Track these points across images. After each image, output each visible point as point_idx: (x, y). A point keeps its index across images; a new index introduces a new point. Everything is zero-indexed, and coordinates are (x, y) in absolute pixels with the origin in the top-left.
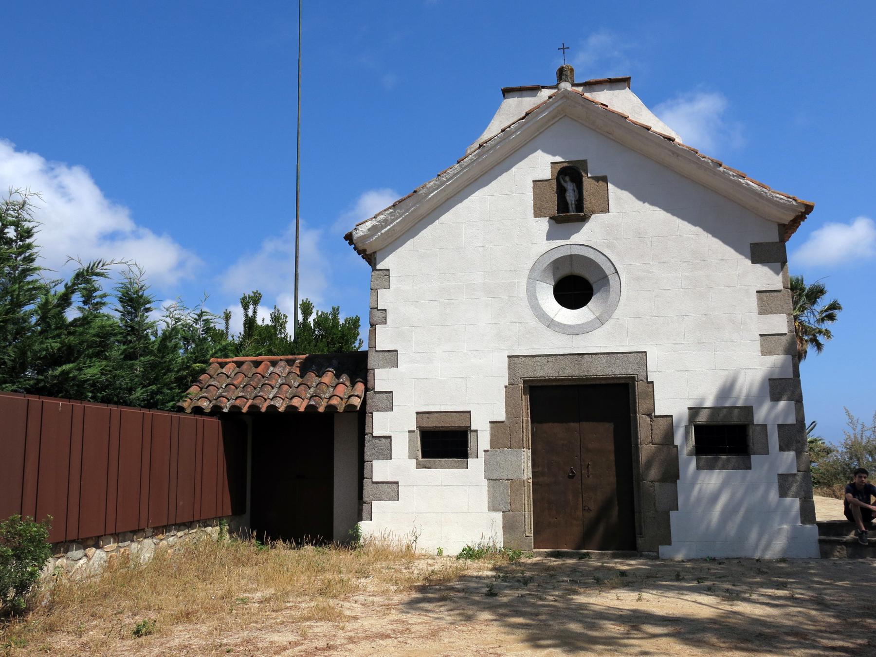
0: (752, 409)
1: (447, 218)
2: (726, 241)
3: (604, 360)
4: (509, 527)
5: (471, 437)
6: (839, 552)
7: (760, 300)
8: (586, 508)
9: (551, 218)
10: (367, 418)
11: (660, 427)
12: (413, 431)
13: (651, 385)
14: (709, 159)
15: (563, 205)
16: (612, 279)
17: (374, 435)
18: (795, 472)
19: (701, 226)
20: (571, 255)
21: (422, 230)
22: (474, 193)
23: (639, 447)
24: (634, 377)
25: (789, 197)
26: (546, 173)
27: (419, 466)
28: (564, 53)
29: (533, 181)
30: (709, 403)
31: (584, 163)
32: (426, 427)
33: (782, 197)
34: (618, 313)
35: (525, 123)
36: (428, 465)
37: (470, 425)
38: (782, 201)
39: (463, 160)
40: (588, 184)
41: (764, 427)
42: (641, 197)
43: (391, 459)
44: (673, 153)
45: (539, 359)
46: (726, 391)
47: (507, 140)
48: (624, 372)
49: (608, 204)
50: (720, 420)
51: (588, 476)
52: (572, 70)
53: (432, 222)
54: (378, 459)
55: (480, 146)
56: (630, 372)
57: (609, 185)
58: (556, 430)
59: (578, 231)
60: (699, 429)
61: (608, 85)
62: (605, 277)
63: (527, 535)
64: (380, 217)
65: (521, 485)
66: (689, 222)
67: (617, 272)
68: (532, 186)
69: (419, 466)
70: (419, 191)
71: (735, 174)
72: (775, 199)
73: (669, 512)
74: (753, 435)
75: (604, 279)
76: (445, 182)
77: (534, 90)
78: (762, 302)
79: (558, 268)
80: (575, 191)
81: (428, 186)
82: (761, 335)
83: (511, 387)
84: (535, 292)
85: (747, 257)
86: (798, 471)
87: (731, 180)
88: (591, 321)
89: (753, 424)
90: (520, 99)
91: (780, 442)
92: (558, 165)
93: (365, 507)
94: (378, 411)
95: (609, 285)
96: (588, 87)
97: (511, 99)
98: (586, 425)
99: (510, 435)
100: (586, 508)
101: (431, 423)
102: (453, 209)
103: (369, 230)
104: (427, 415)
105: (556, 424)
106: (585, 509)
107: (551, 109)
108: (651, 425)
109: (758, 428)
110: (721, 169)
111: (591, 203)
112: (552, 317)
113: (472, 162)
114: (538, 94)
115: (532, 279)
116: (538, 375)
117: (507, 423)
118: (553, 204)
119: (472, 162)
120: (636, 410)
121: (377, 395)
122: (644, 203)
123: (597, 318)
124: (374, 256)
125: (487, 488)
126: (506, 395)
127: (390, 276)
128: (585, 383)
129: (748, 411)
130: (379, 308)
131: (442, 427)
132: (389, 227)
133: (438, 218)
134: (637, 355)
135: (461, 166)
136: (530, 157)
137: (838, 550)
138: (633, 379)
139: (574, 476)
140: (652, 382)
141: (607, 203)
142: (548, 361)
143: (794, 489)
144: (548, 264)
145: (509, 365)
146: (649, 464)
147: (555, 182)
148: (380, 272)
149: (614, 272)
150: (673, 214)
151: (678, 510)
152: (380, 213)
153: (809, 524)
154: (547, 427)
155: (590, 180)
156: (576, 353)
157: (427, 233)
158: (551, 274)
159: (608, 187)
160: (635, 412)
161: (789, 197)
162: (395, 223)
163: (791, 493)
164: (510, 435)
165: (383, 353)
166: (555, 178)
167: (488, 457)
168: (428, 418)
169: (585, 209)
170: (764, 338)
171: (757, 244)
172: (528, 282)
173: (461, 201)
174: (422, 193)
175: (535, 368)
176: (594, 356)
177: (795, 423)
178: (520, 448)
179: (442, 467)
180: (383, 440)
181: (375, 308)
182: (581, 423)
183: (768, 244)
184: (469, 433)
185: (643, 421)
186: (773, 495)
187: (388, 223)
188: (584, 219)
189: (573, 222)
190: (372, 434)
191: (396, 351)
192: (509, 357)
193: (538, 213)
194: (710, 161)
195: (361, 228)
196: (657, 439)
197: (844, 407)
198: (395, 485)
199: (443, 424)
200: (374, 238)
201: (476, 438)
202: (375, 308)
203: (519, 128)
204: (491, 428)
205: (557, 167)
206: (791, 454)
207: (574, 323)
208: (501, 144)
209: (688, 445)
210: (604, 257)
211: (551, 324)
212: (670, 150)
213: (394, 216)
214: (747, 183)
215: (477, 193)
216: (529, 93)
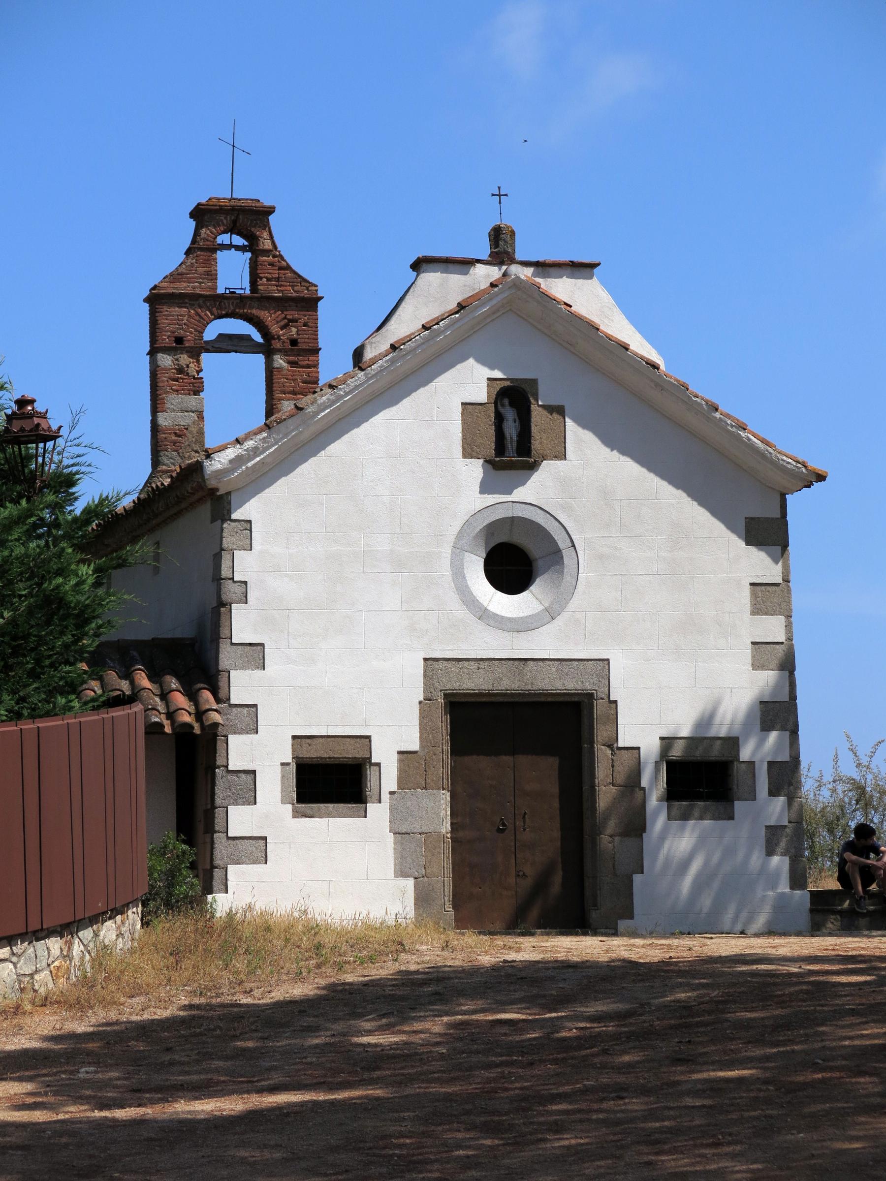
0: (738, 741)
1: (337, 448)
2: (714, 513)
3: (554, 669)
4: (422, 899)
5: (371, 774)
6: (833, 923)
7: (754, 595)
8: (521, 873)
9: (486, 461)
10: (219, 743)
11: (624, 762)
12: (288, 764)
13: (613, 706)
14: (702, 399)
15: (500, 446)
16: (567, 554)
17: (231, 768)
18: (786, 823)
19: (685, 490)
20: (513, 517)
21: (301, 464)
22: (377, 414)
23: (596, 789)
24: (592, 694)
25: (798, 462)
26: (480, 394)
27: (297, 814)
28: (500, 203)
29: (463, 404)
30: (685, 732)
31: (534, 382)
32: (307, 758)
33: (790, 460)
34: (575, 603)
35: (458, 320)
36: (309, 812)
37: (369, 756)
38: (789, 466)
39: (370, 366)
40: (538, 415)
41: (751, 764)
42: (610, 441)
43: (255, 803)
44: (657, 385)
45: (466, 664)
46: (706, 721)
47: (431, 342)
48: (579, 686)
49: (565, 448)
50: (698, 754)
51: (524, 830)
52: (513, 233)
53: (315, 454)
54: (236, 803)
55: (393, 347)
56: (588, 687)
57: (567, 420)
58: (483, 764)
59: (523, 483)
60: (673, 767)
61: (569, 270)
62: (558, 552)
63: (447, 909)
64: (248, 443)
65: (440, 841)
66: (671, 482)
67: (574, 546)
68: (460, 410)
69: (297, 814)
70: (307, 409)
71: (734, 424)
72: (781, 462)
73: (632, 876)
74: (738, 771)
75: (555, 556)
76: (342, 397)
77: (465, 264)
78: (756, 598)
79: (493, 534)
80: (515, 422)
81: (319, 402)
82: (753, 643)
83: (427, 703)
84: (463, 568)
85: (740, 537)
86: (790, 822)
87: (728, 431)
88: (538, 614)
89: (738, 760)
90: (444, 275)
91: (769, 784)
92: (498, 382)
93: (217, 873)
94: (235, 733)
95: (563, 564)
96: (540, 269)
97: (432, 274)
98: (523, 760)
99: (426, 771)
100: (521, 873)
101: (312, 753)
102: (346, 436)
103: (231, 461)
104: (308, 741)
105: (481, 757)
106: (519, 875)
107: (494, 302)
108: (613, 760)
109: (743, 766)
110: (717, 415)
111: (541, 443)
112: (485, 604)
113: (381, 370)
114: (471, 272)
115: (458, 548)
116: (465, 686)
117: (421, 754)
118: (489, 441)
119: (382, 370)
120: (593, 738)
121: (234, 710)
122: (612, 450)
123: (546, 609)
124: (227, 498)
125: (393, 845)
126: (420, 713)
127: (253, 530)
128: (525, 700)
129: (732, 743)
130: (235, 580)
131: (330, 758)
132: (258, 459)
133: (324, 449)
134: (597, 664)
135: (366, 375)
136: (459, 366)
137: (832, 920)
138: (590, 696)
139: (505, 830)
140: (615, 702)
141: (563, 445)
142: (479, 668)
143: (783, 844)
144: (481, 528)
145: (425, 671)
146: (609, 810)
147: (492, 408)
148: (237, 523)
149: (570, 545)
150: (650, 469)
151: (642, 873)
152: (248, 437)
153: (799, 889)
154: (468, 760)
155: (540, 409)
156: (517, 657)
157: (307, 469)
158: (483, 543)
159: (565, 423)
160: (591, 743)
161: (798, 462)
162: (267, 453)
163: (779, 850)
164: (426, 771)
165: (243, 647)
166: (493, 401)
167: (395, 802)
168: (310, 745)
169: (533, 452)
170: (757, 646)
171: (752, 519)
172: (453, 552)
173: (358, 425)
174: (309, 412)
175: (460, 677)
176: (540, 663)
177: (788, 759)
178: (439, 789)
179: (329, 815)
180: (243, 776)
181: (230, 579)
182: (516, 756)
183: (767, 520)
184: (368, 767)
185: (602, 753)
186: (756, 858)
187: (258, 452)
188: (533, 467)
189: (518, 469)
190: (227, 767)
191: (262, 645)
192: (425, 660)
193: (468, 452)
194: (703, 403)
195: (218, 457)
196: (620, 779)
197: (836, 748)
198: (262, 842)
199: (331, 754)
200: (236, 474)
201: (378, 774)
202: (230, 579)
203: (449, 327)
204: (400, 761)
205: (495, 385)
206: (781, 800)
207: (515, 616)
208: (424, 346)
209: (658, 787)
210: (557, 524)
211: (484, 615)
212: (652, 381)
213: (268, 442)
214: (748, 437)
215: (381, 415)
216: (458, 267)
